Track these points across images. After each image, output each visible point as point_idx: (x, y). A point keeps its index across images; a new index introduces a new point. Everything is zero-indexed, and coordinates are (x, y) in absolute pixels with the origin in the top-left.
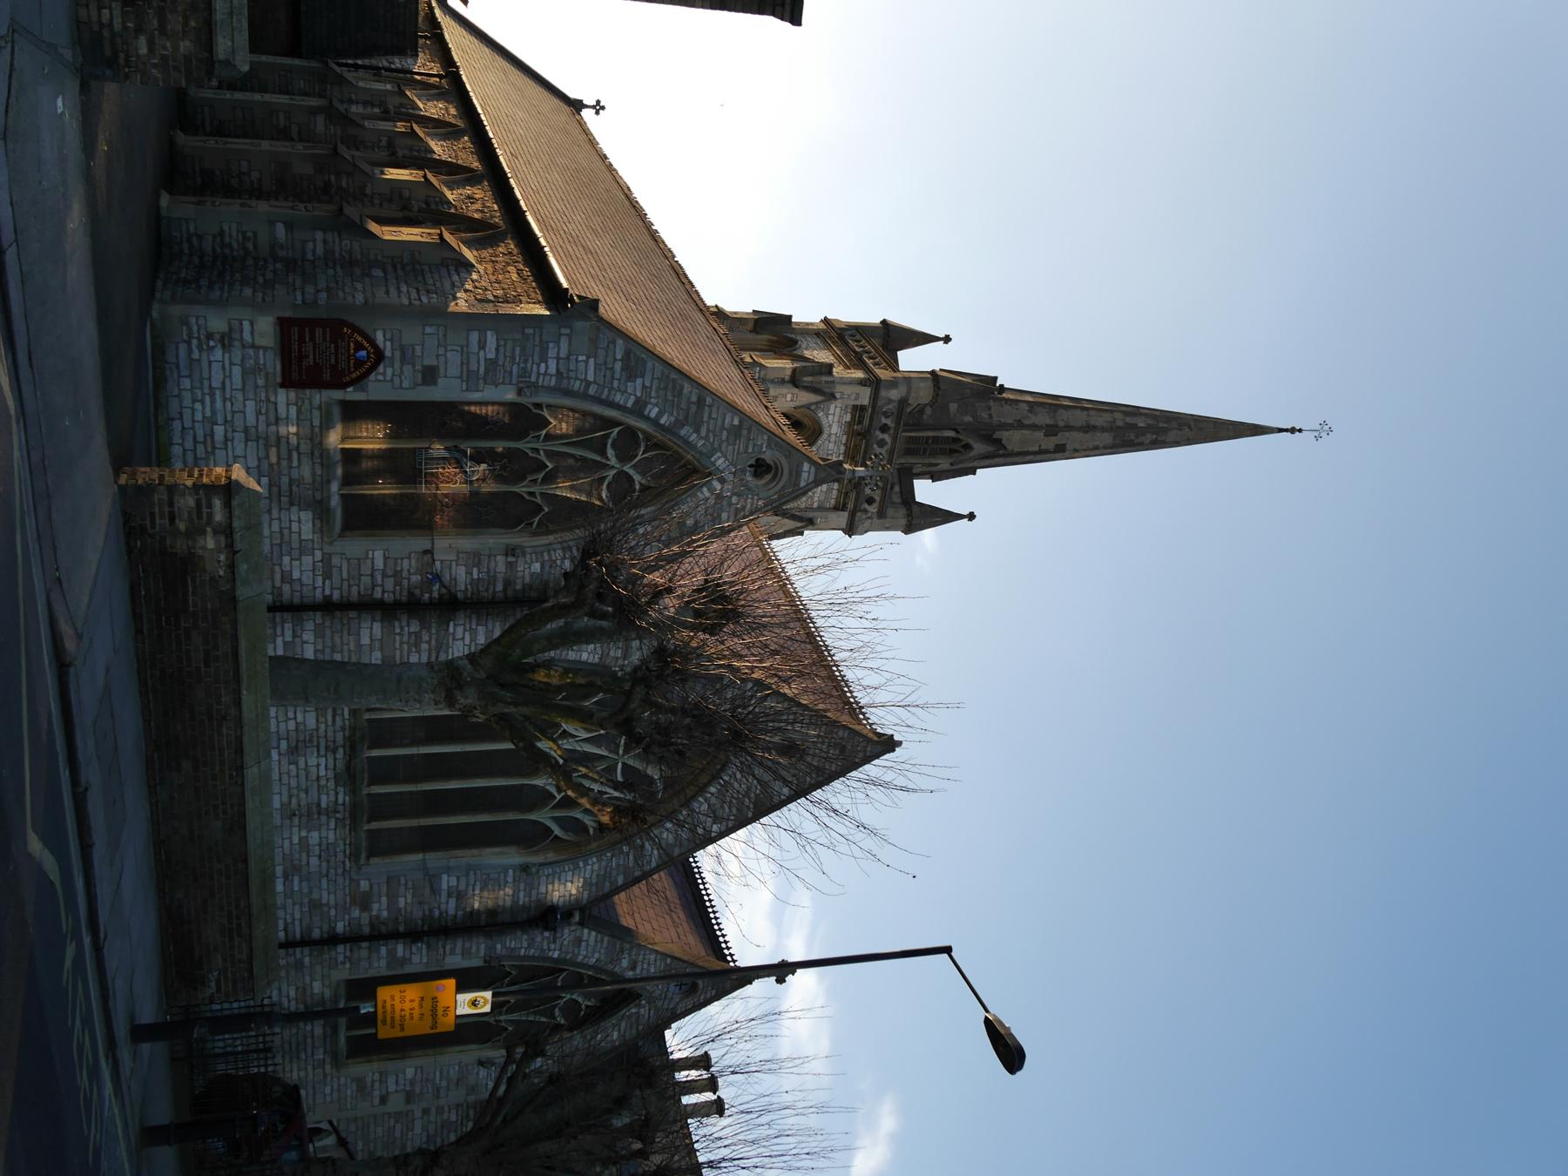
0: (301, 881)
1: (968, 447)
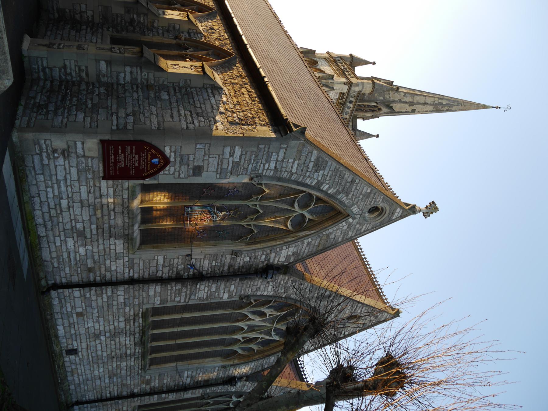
0: (117, 378)
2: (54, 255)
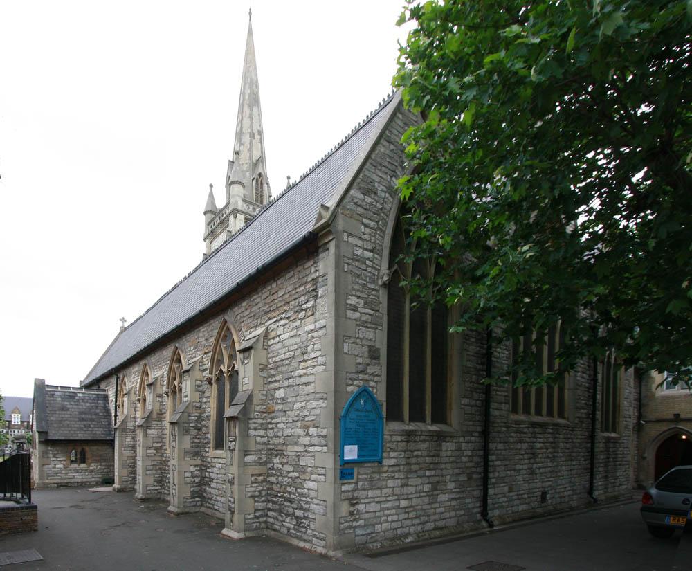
1: (260, 175)
2: (453, 514)
